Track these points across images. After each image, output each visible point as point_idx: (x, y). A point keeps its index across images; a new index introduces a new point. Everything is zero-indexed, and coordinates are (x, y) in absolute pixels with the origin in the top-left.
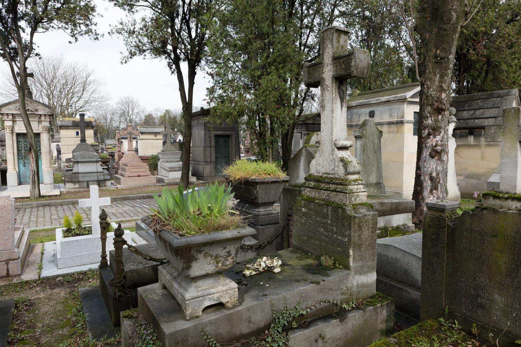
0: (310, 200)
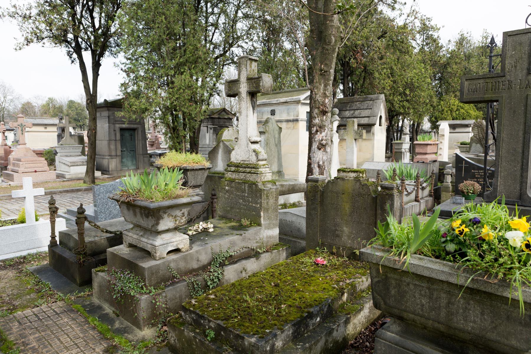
0: (232, 181)
